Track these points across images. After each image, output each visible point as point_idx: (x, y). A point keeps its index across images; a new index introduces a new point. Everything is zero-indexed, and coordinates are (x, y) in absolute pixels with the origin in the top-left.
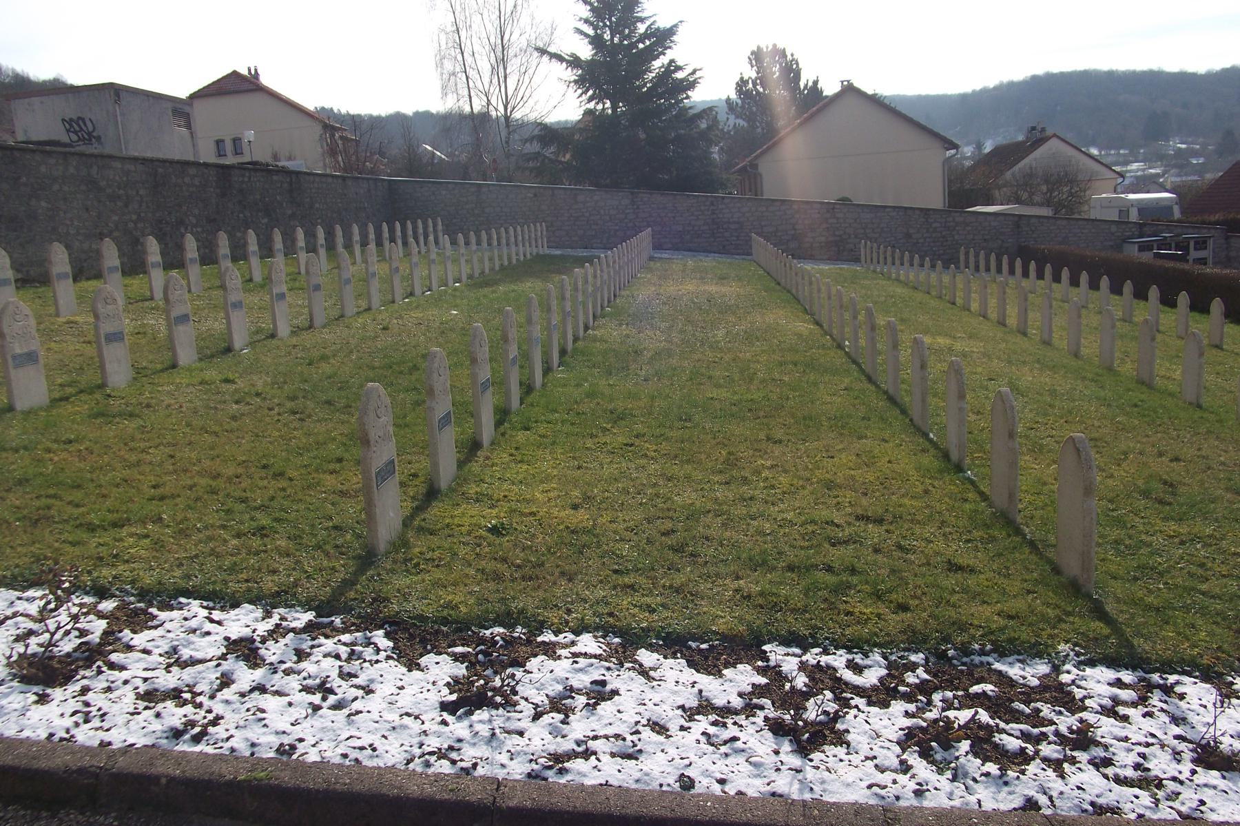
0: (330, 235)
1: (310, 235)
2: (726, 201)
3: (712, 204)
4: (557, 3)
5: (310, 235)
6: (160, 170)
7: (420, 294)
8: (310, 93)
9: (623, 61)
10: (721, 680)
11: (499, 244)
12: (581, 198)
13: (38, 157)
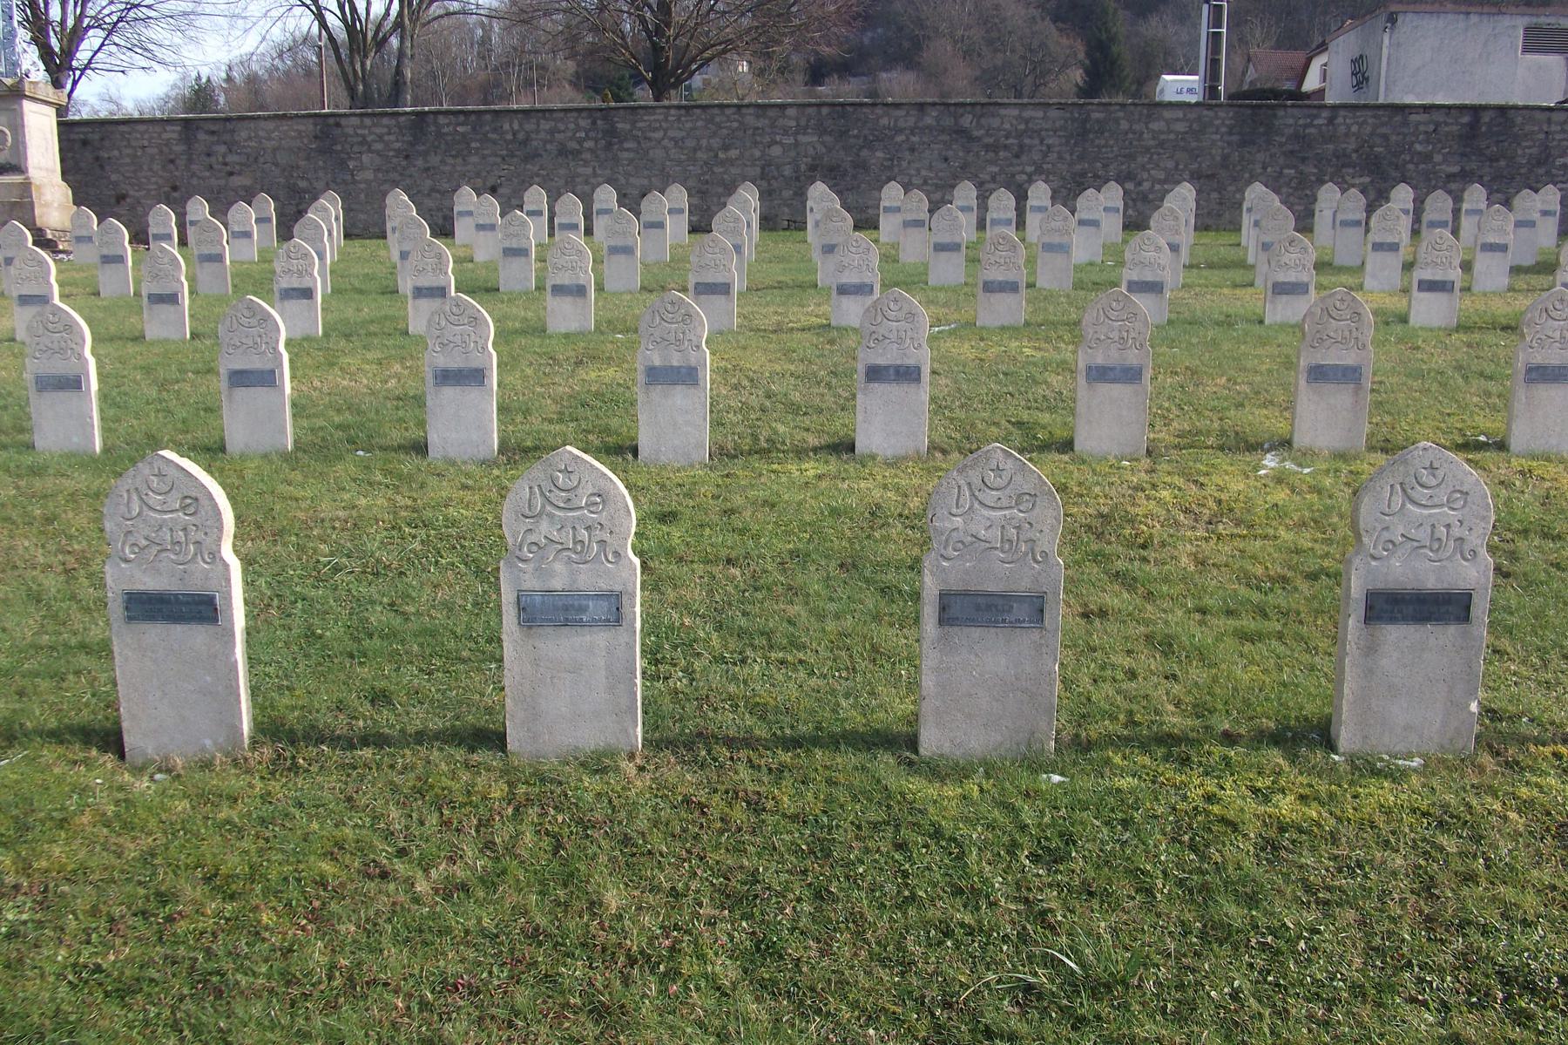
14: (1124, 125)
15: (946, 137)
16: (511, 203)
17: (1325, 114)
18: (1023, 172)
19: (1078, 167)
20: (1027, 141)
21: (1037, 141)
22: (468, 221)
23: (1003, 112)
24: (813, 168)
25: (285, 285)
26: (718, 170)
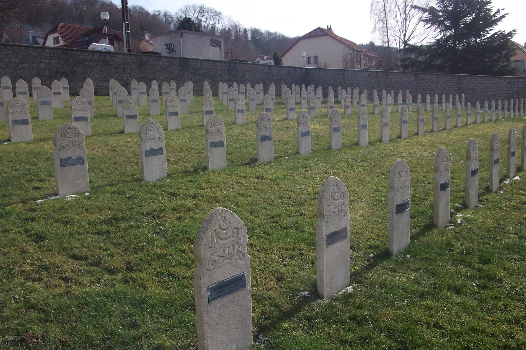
0: (454, 98)
1: (432, 97)
2: (467, 78)
3: (458, 79)
5: (432, 97)
7: (307, 117)
8: (335, 33)
11: (503, 109)
12: (390, 76)
13: (79, 53)
14: (152, 62)
15: (101, 64)
16: (230, 86)
17: (200, 62)
18: (125, 76)
19: (141, 75)
20: (126, 66)
21: (129, 66)
22: (136, 91)
23: (118, 56)
24: (57, 72)
25: (170, 111)
26: (19, 72)
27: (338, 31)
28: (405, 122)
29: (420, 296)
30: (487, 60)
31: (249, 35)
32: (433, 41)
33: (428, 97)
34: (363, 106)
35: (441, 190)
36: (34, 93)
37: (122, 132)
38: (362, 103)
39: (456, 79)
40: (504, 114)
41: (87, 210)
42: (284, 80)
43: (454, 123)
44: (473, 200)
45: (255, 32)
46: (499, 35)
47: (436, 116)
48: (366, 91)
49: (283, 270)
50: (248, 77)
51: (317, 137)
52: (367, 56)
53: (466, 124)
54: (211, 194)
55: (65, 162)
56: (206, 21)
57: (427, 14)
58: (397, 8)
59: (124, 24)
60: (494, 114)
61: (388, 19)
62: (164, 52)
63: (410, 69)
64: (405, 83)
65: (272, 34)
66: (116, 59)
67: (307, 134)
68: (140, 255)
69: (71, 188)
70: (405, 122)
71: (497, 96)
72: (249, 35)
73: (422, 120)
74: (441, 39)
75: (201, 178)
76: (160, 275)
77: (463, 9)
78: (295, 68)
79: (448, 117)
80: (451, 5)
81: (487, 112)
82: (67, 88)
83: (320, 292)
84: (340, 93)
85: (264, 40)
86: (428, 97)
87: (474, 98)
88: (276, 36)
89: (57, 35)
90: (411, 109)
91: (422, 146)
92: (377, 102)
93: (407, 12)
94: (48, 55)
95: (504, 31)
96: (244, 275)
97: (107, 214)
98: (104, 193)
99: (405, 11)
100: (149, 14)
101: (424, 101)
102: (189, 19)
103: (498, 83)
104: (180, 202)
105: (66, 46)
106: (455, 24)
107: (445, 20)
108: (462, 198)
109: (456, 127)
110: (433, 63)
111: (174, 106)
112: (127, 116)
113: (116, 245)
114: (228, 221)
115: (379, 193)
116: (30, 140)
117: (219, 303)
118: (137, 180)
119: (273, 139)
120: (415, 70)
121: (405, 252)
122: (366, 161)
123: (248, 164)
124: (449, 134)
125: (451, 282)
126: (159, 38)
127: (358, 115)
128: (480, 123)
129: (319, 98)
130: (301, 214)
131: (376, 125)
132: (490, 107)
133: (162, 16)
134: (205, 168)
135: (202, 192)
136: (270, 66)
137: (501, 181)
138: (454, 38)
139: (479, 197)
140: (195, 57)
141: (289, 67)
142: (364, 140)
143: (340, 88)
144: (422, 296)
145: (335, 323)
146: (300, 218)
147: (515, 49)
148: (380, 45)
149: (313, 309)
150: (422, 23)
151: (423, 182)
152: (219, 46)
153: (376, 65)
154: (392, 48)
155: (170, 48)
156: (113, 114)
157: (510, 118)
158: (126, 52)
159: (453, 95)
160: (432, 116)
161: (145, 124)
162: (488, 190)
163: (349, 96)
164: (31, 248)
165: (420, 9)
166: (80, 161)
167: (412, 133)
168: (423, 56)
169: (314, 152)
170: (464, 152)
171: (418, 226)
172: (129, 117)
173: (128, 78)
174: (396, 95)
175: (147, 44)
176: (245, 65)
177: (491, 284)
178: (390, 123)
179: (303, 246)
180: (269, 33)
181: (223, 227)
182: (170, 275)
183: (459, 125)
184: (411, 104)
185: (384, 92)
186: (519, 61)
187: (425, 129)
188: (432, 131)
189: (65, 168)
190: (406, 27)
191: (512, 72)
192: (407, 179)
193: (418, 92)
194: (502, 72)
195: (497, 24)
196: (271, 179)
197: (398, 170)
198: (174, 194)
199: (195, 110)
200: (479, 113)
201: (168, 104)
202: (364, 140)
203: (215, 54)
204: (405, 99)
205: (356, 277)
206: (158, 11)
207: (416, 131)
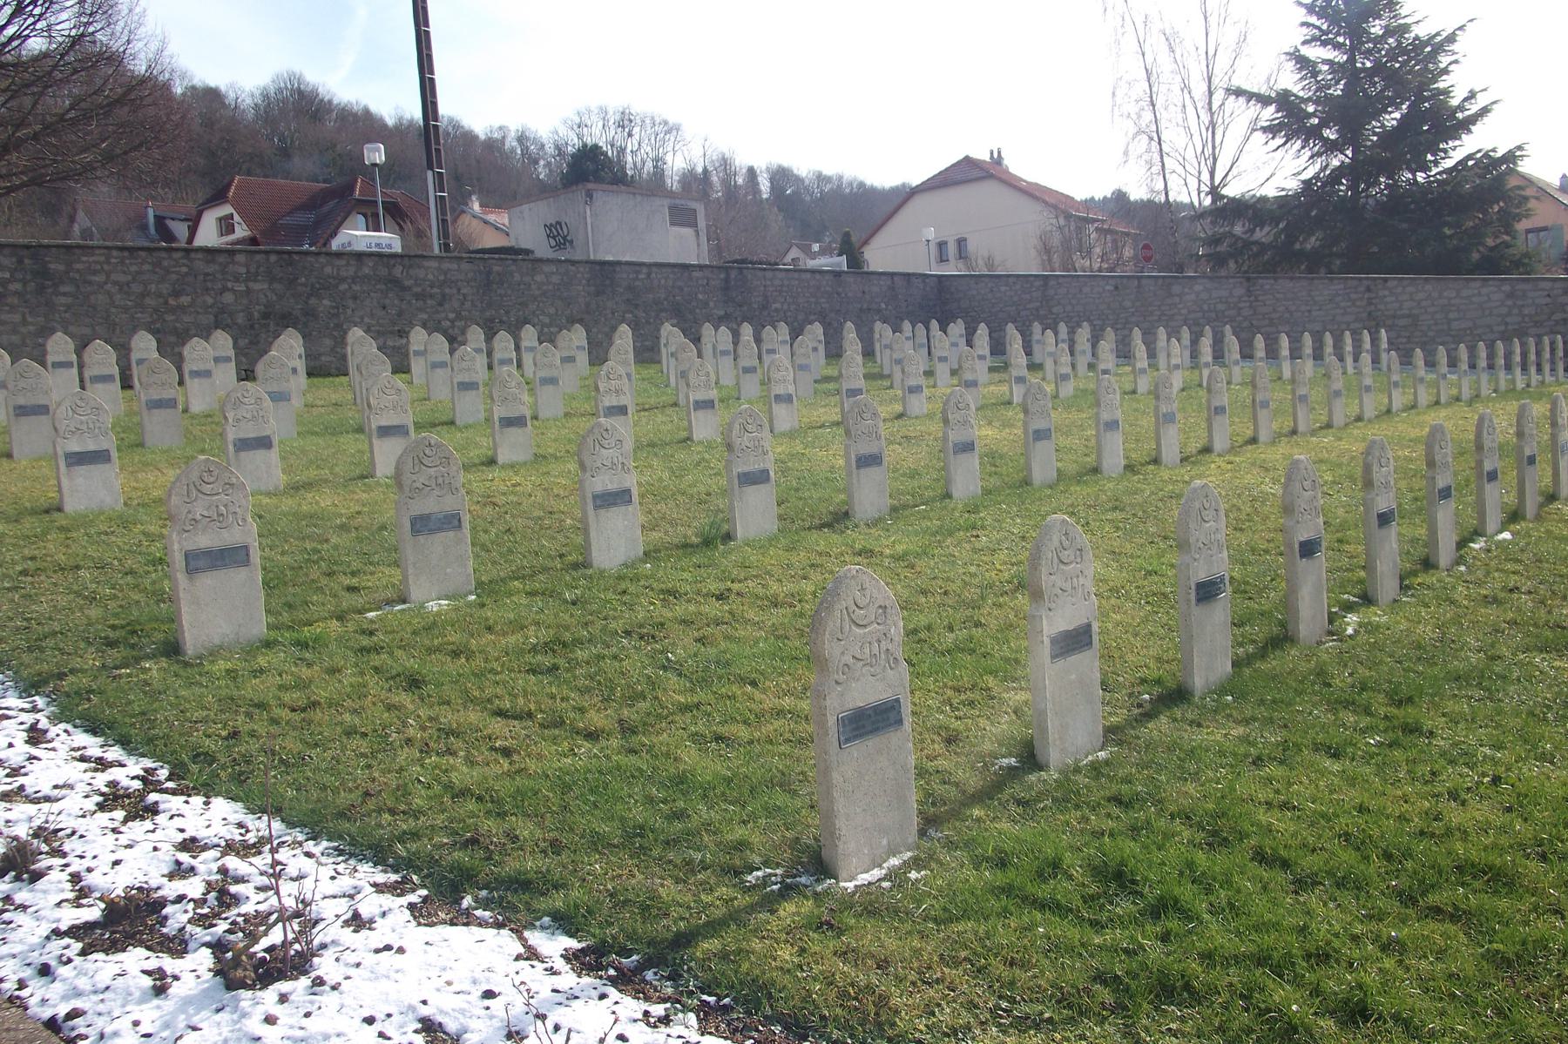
2: (1389, 284)
3: (1368, 289)
4: (1269, 25)
6: (496, 268)
9: (1378, 97)
10: (425, 1011)
11: (1491, 367)
13: (322, 259)
14: (517, 277)
20: (447, 291)
22: (421, 360)
24: (266, 316)
26: (169, 318)
27: (1021, 166)
28: (1220, 410)
29: (1254, 763)
30: (1447, 231)
31: (764, 185)
32: (1293, 185)
33: (1284, 342)
34: (1105, 372)
35: (1302, 556)
36: (527, 359)
37: (491, 462)
38: (1102, 366)
39: (1362, 289)
40: (1497, 383)
41: (489, 628)
42: (879, 311)
43: (1354, 410)
44: (1387, 587)
45: (781, 176)
46: (1478, 162)
47: (1302, 391)
48: (1110, 333)
49: (956, 724)
50: (778, 305)
51: (992, 457)
52: (1109, 231)
53: (1389, 411)
54: (760, 591)
55: (422, 525)
56: (638, 154)
57: (1272, 108)
58: (1187, 96)
59: (430, 173)
60: (1465, 383)
61: (1162, 125)
62: (542, 247)
63: (1232, 265)
64: (1220, 307)
65: (828, 179)
66: (421, 273)
67: (968, 447)
68: (643, 705)
69: (436, 585)
70: (1220, 410)
71: (1479, 331)
72: (764, 185)
73: (1265, 405)
74: (1316, 177)
75: (727, 559)
76: (696, 738)
77: (1373, 92)
78: (907, 276)
79: (1337, 394)
80: (1337, 83)
81: (1444, 376)
82: (228, 359)
83: (1040, 758)
84: (1038, 342)
85: (808, 198)
86: (1284, 342)
87: (1413, 340)
88: (840, 186)
89: (227, 210)
90: (1237, 378)
91: (1267, 470)
92: (1142, 361)
93: (1215, 107)
94: (243, 270)
95: (1494, 150)
96: (897, 700)
97: (545, 635)
98: (510, 594)
99: (1210, 103)
100: (477, 137)
101: (1272, 353)
102: (596, 147)
103: (1479, 294)
104: (692, 608)
105: (253, 241)
106: (1351, 136)
107: (1324, 123)
108: (1361, 582)
109: (1359, 419)
110: (1297, 246)
111: (617, 392)
112: (501, 419)
113: (583, 691)
114: (868, 593)
115: (1156, 579)
116: (276, 488)
117: (857, 749)
118: (576, 566)
119: (885, 463)
120: (1245, 268)
121: (1222, 690)
122: (1122, 510)
123: (829, 525)
124: (1340, 439)
125: (1320, 738)
126: (525, 207)
127: (1095, 399)
128: (1429, 407)
129: (982, 358)
130: (978, 624)
131: (1144, 423)
132: (1453, 363)
133: (511, 143)
134: (728, 537)
135: (736, 587)
136: (837, 274)
137: (1462, 544)
138: (1357, 172)
139: (1402, 579)
140: (627, 258)
141: (892, 275)
142: (1114, 460)
143: (1037, 327)
144: (1258, 762)
145: (1077, 807)
146: (977, 632)
147: (1526, 199)
148: (1145, 197)
149: (1031, 787)
150: (1259, 137)
151: (1266, 551)
152: (694, 225)
153: (1135, 257)
154: (1180, 206)
155: (558, 234)
156: (444, 418)
157: (1514, 389)
158: (437, 251)
159: (1313, 334)
160: (1293, 392)
161: (591, 431)
162: (1428, 564)
163: (1065, 346)
164: (404, 698)
165: (1250, 96)
166: (452, 521)
167: (1240, 439)
168: (1267, 229)
169: (987, 492)
170: (1359, 472)
171: (1254, 641)
172: (508, 422)
173: (452, 322)
174: (1195, 342)
175: (475, 222)
176: (769, 274)
177: (1406, 740)
178: (1179, 416)
179: (991, 681)
180: (821, 178)
181: (859, 602)
182: (719, 738)
183: (1369, 413)
184: (1237, 363)
185: (1162, 333)
186: (1545, 229)
187: (1275, 426)
188: (1294, 432)
189: (421, 539)
190: (1214, 147)
191: (1521, 264)
192: (1216, 528)
193: (1255, 329)
194: (1493, 265)
195: (1470, 131)
196: (892, 556)
197: (1197, 505)
198: (673, 593)
199: (653, 401)
200: (1422, 380)
201: (602, 386)
202: (1114, 460)
203: (681, 246)
204: (1222, 350)
205: (1112, 734)
206: (501, 128)
207: (1249, 433)
